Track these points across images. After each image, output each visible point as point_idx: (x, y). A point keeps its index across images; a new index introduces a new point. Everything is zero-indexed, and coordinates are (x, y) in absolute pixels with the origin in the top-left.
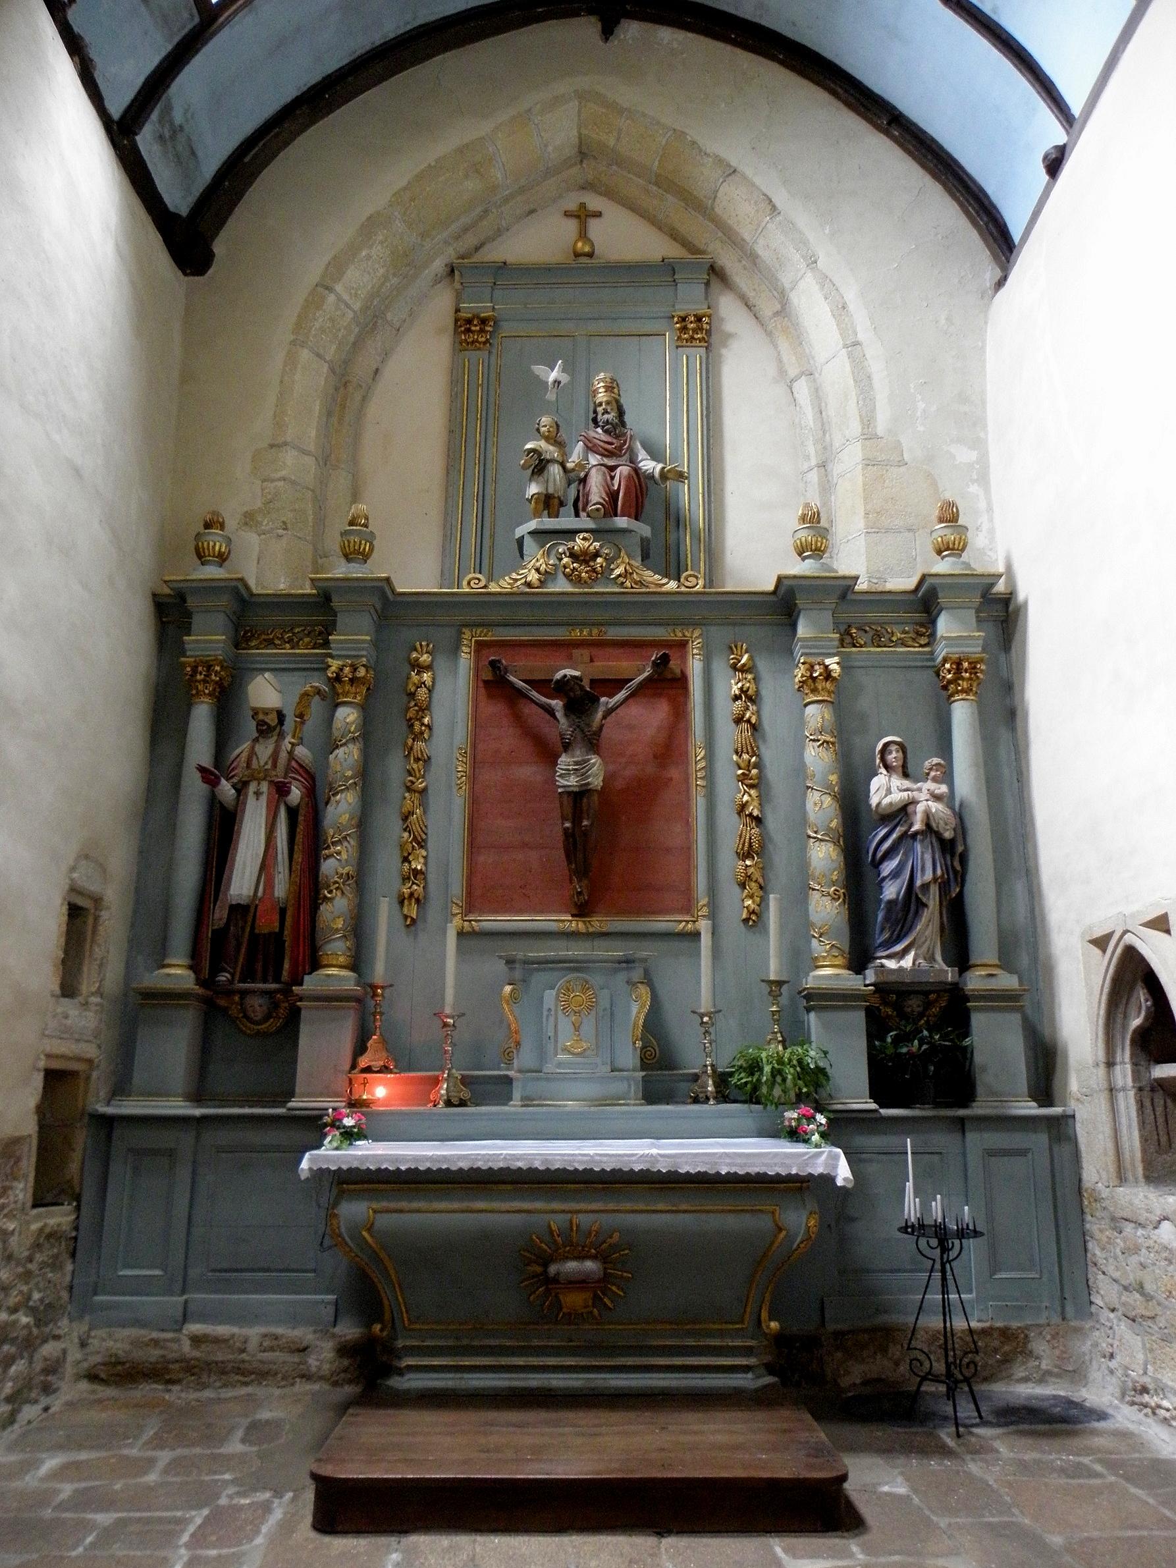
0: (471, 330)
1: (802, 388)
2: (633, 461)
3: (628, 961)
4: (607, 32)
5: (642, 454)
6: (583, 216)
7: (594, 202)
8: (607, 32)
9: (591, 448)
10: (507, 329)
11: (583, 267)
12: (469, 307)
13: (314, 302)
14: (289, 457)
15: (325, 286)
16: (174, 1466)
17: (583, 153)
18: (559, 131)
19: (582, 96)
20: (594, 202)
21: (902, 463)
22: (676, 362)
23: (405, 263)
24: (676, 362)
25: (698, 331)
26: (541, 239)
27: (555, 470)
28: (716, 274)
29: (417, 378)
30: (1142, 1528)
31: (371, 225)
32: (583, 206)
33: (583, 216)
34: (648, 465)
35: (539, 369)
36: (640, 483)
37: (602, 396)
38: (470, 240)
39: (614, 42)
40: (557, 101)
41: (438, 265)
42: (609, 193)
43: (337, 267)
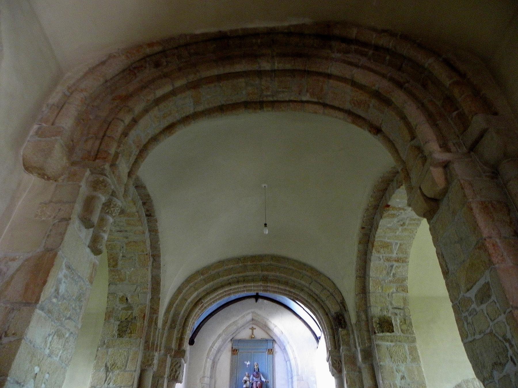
0: (234, 351)
1: (288, 362)
2: (261, 379)
3: (355, 382)
4: (256, 301)
5: (262, 377)
6: (253, 329)
7: (254, 326)
8: (256, 301)
9: (254, 376)
10: (240, 351)
11: (252, 340)
12: (234, 347)
13: (210, 350)
14: (206, 379)
15: (212, 347)
16: (386, 266)
17: (253, 320)
18: (249, 317)
19: (253, 312)
20: (254, 326)
21: (303, 380)
22: (268, 357)
23: (224, 341)
24: (268, 357)
25: (271, 351)
26: (245, 334)
27: (248, 382)
28: (274, 341)
29: (225, 360)
30: (50, 345)
31: (220, 336)
32: (257, 294)
33: (253, 329)
34: (263, 379)
35: (246, 362)
36: (262, 382)
37: (256, 367)
38: (234, 335)
39: (257, 303)
40: (249, 313)
41: (229, 339)
42: (257, 325)
43: (214, 344)
